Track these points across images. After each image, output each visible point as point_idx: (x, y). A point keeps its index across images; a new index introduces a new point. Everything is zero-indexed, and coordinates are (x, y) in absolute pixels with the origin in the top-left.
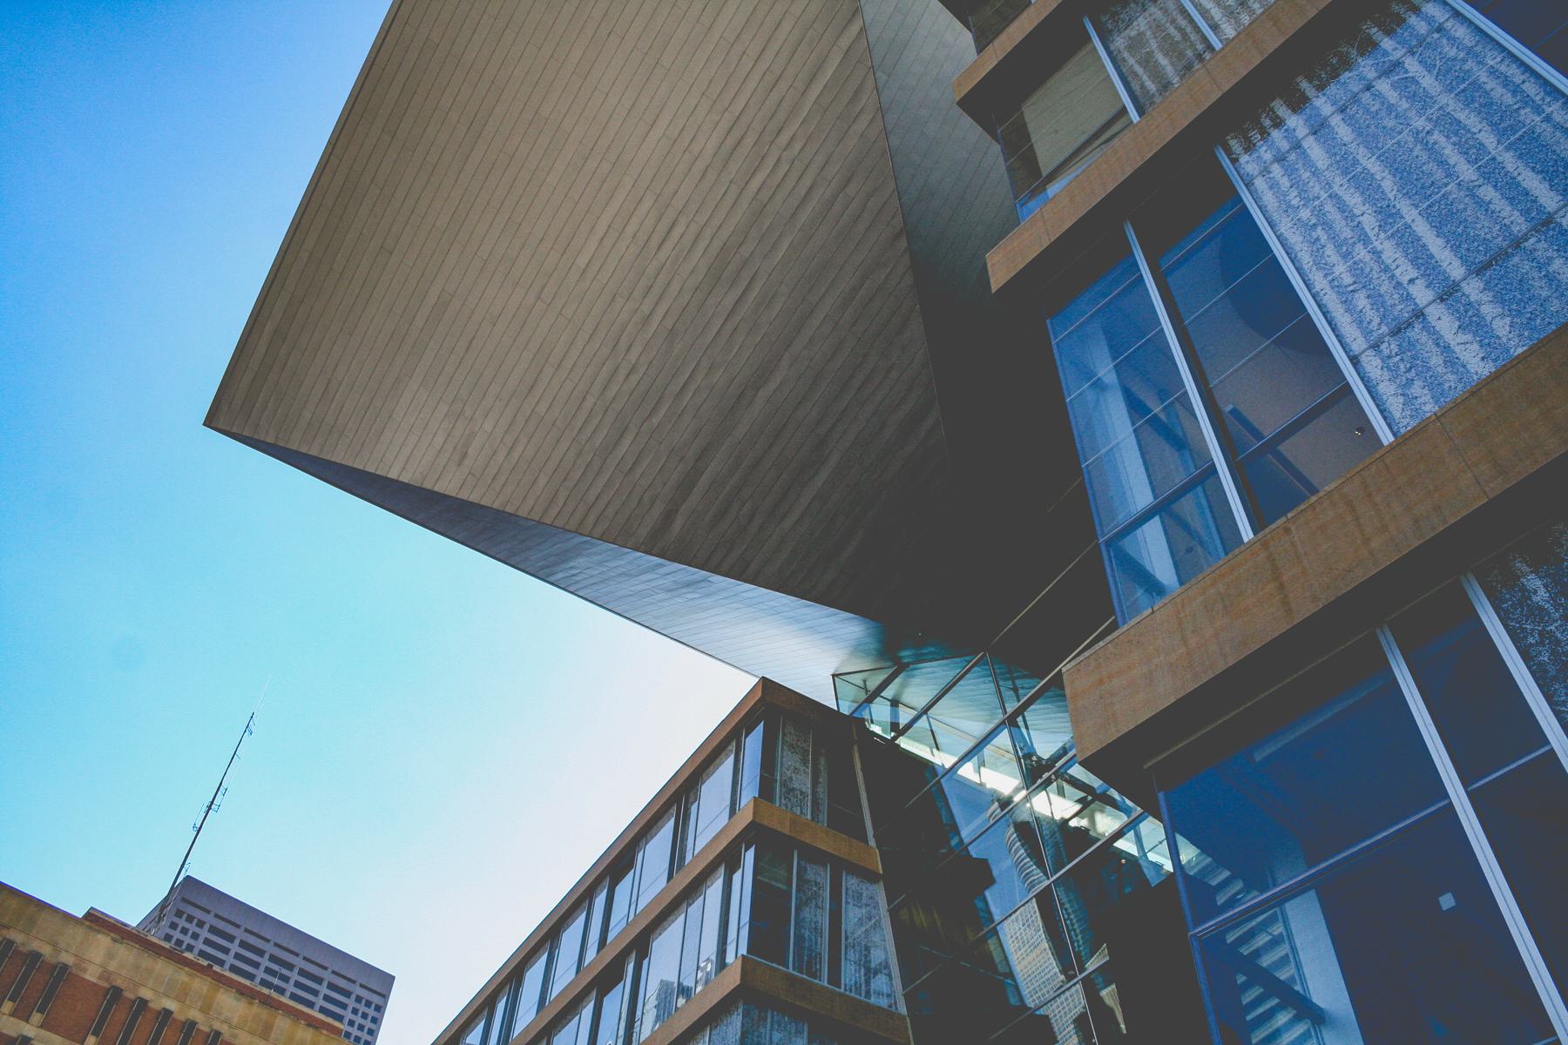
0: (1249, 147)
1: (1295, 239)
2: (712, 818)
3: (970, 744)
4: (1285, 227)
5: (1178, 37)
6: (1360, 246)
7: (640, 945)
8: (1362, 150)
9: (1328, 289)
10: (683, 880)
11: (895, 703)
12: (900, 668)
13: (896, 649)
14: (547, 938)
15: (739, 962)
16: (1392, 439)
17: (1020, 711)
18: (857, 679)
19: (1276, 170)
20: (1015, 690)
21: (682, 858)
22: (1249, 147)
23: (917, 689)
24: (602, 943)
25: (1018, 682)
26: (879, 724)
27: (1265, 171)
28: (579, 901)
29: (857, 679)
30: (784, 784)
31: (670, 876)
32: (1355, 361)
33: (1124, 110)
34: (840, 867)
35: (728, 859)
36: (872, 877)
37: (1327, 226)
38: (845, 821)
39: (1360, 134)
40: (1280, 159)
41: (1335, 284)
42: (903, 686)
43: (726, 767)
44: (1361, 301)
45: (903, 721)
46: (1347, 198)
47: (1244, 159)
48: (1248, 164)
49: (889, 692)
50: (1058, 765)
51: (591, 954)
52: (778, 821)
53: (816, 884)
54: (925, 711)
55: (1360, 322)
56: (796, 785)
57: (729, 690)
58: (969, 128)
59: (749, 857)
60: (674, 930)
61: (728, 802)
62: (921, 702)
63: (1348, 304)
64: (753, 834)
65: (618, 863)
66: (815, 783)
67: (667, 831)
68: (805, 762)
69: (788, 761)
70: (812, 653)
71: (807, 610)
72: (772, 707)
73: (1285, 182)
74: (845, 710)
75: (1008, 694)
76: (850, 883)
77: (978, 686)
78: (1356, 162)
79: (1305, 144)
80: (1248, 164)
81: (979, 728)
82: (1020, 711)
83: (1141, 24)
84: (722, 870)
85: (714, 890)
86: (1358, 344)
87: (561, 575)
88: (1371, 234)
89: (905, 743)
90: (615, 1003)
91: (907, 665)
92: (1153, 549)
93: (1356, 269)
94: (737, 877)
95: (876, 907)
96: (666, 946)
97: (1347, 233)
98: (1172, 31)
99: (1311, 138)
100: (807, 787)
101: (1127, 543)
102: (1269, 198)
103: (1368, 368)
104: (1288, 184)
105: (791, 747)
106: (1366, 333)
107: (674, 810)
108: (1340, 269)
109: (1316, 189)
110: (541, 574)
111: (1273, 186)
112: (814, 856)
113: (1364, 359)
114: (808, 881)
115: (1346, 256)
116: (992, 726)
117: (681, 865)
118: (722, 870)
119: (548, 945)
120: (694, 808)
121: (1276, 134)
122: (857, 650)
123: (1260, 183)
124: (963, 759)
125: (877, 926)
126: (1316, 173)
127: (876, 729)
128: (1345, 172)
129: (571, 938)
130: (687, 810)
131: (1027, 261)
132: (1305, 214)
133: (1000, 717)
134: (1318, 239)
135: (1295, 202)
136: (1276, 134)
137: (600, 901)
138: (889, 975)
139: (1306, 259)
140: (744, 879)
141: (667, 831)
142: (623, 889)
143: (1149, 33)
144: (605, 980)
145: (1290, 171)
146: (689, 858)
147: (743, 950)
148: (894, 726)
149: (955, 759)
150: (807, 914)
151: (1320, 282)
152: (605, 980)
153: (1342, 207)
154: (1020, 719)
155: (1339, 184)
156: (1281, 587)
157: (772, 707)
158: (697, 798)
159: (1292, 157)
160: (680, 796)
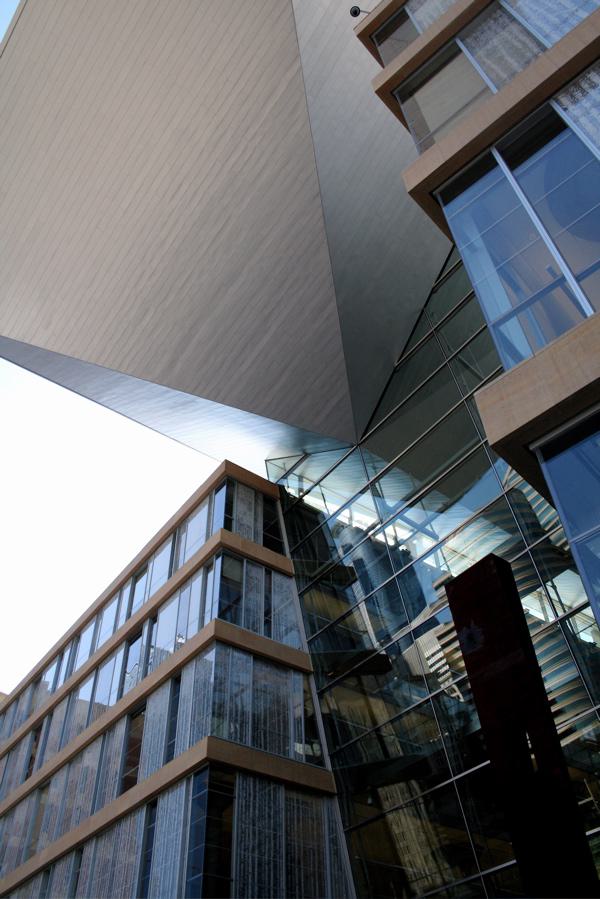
0: (575, 101)
2: (196, 540)
3: (344, 502)
5: (520, 46)
7: (153, 616)
10: (178, 578)
11: (301, 478)
12: (306, 455)
13: (304, 443)
14: (96, 612)
15: (214, 622)
17: (377, 479)
20: (375, 468)
21: (177, 566)
23: (313, 470)
24: (129, 615)
25: (376, 464)
27: (587, 113)
28: (116, 591)
29: (279, 463)
31: (206, 540)
33: (487, 88)
34: (270, 570)
35: (206, 565)
38: (272, 542)
42: (307, 467)
43: (203, 512)
45: (306, 488)
49: (297, 471)
50: (370, 533)
51: (122, 622)
52: (235, 541)
54: (318, 483)
57: (205, 471)
58: (381, 107)
59: (218, 563)
62: (316, 478)
64: (224, 551)
65: (138, 571)
66: (256, 520)
67: (167, 549)
68: (250, 509)
69: (239, 508)
70: (256, 447)
71: (252, 420)
72: (231, 478)
74: (272, 480)
75: (370, 471)
76: (276, 578)
77: (352, 466)
80: (574, 110)
81: (349, 495)
82: (377, 479)
83: (495, 41)
84: (124, 644)
85: (197, 583)
87: (105, 399)
89: (309, 500)
90: (137, 648)
91: (310, 454)
92: (514, 331)
94: (211, 575)
95: (291, 592)
96: (167, 616)
98: (516, 44)
101: (502, 328)
105: (242, 500)
107: (172, 536)
110: (94, 398)
112: (255, 562)
116: (354, 494)
117: (176, 569)
118: (124, 644)
119: (118, 594)
120: (183, 536)
122: (281, 445)
123: (583, 120)
124: (343, 507)
125: (292, 603)
127: (289, 490)
129: (109, 613)
130: (179, 538)
131: (429, 173)
133: (365, 483)
137: (127, 592)
138: (299, 631)
140: (215, 577)
141: (167, 549)
142: (141, 584)
143: (500, 46)
144: (132, 636)
146: (181, 565)
147: (215, 615)
148: (301, 490)
149: (338, 508)
150: (251, 596)
152: (132, 636)
158: (185, 530)
160: (175, 531)
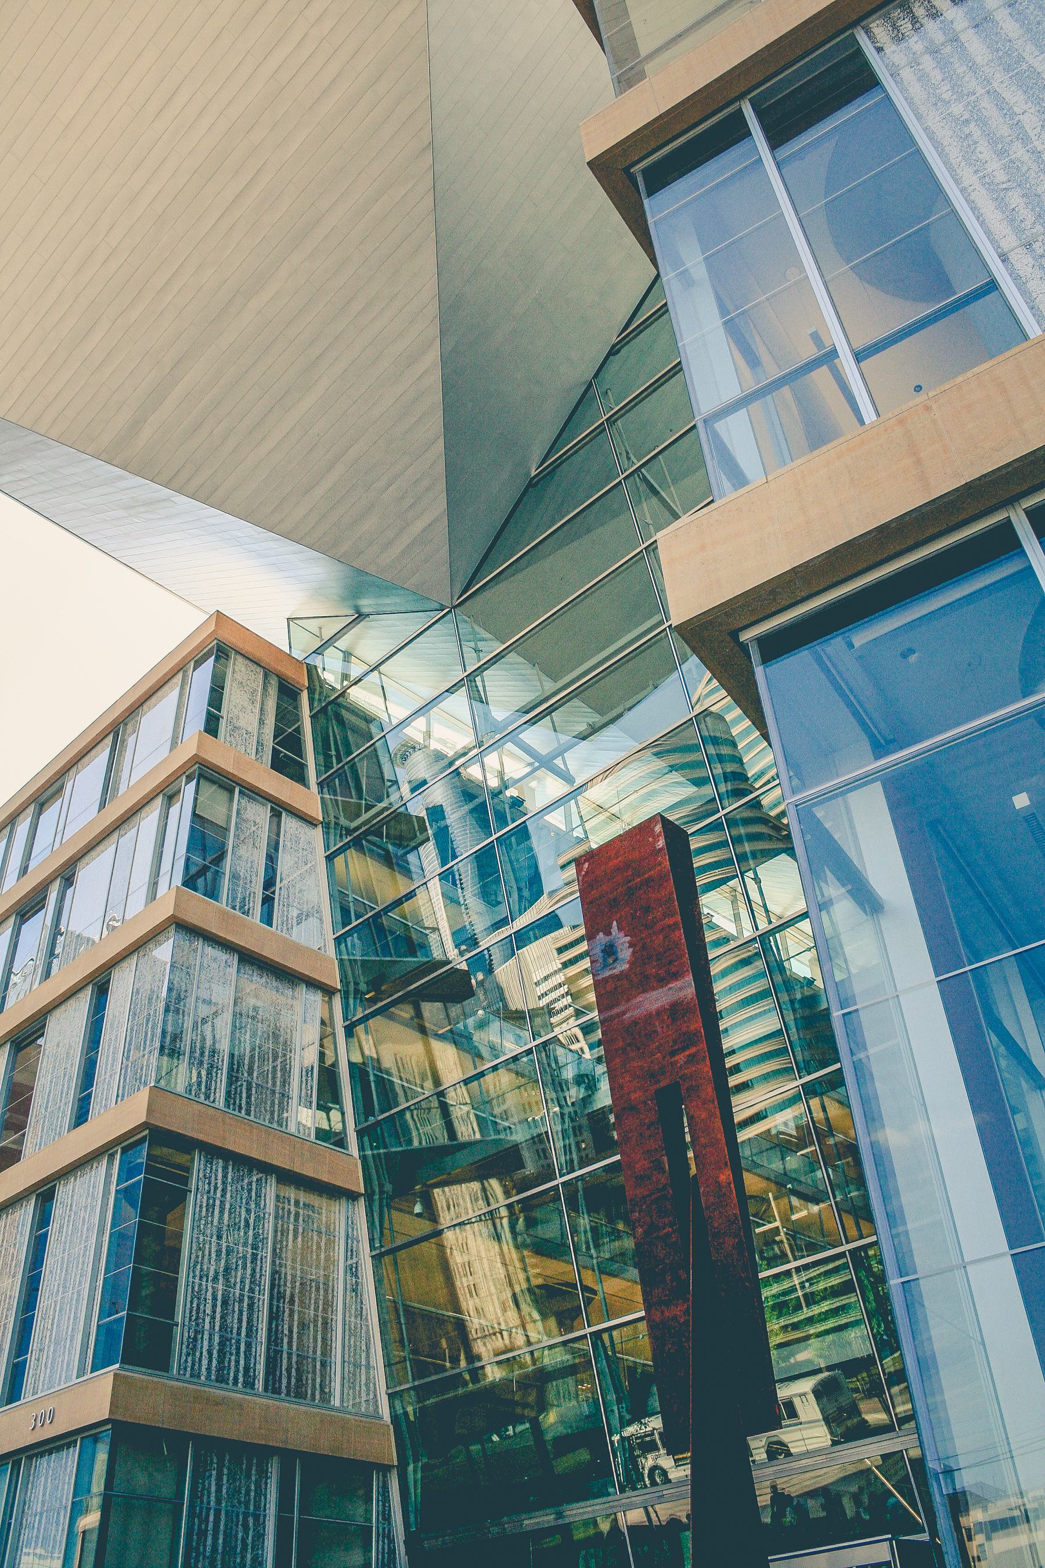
1: (944, 133)
2: (156, 748)
3: (423, 703)
4: (933, 119)
6: (1017, 145)
8: (1029, 47)
9: (977, 186)
10: (116, 810)
11: (347, 655)
16: (1039, 332)
17: (480, 670)
18: (313, 625)
19: (928, 63)
20: (477, 651)
22: (899, 38)
23: (370, 642)
26: (332, 672)
30: (230, 722)
31: (102, 805)
32: (1004, 258)
34: (279, 809)
36: (311, 822)
37: (983, 122)
39: (1029, 30)
40: (933, 51)
41: (990, 185)
44: (1015, 199)
46: (1007, 95)
47: (890, 48)
48: (895, 53)
49: (342, 643)
53: (255, 824)
55: (1011, 218)
56: (241, 723)
60: (104, 857)
61: (170, 734)
62: (374, 658)
63: (1001, 203)
66: (261, 722)
67: (101, 758)
72: (221, 647)
73: (936, 76)
75: (470, 655)
76: (289, 824)
77: (440, 642)
78: (1021, 59)
79: (963, 37)
80: (895, 53)
82: (480, 670)
85: (150, 820)
86: (1009, 241)
88: (1032, 134)
93: (1012, 167)
94: (175, 810)
96: (92, 876)
97: (1005, 131)
99: (971, 32)
100: (253, 726)
102: (916, 90)
103: (1018, 265)
104: (939, 78)
106: (1019, 231)
108: (994, 166)
109: (972, 83)
111: (923, 78)
112: (252, 793)
113: (1013, 257)
114: (246, 821)
115: (1001, 153)
121: (931, 26)
123: (906, 74)
126: (973, 68)
128: (1007, 70)
132: (957, 109)
134: (970, 135)
135: (946, 96)
136: (931, 26)
137: (23, 828)
139: (954, 153)
141: (102, 756)
145: (943, 64)
148: (345, 676)
149: (408, 713)
150: (242, 851)
151: (969, 177)
153: (1001, 104)
154: (478, 679)
155: (999, 80)
156: (919, 462)
157: (221, 647)
159: (948, 49)
160: (116, 730)
